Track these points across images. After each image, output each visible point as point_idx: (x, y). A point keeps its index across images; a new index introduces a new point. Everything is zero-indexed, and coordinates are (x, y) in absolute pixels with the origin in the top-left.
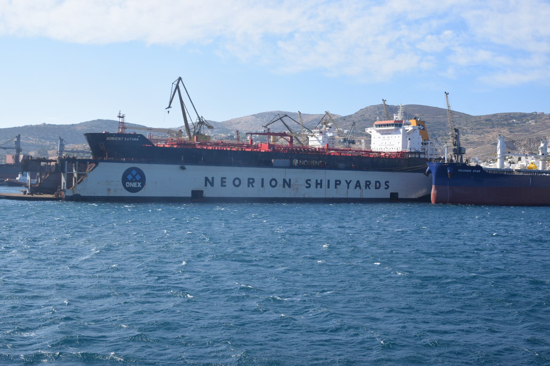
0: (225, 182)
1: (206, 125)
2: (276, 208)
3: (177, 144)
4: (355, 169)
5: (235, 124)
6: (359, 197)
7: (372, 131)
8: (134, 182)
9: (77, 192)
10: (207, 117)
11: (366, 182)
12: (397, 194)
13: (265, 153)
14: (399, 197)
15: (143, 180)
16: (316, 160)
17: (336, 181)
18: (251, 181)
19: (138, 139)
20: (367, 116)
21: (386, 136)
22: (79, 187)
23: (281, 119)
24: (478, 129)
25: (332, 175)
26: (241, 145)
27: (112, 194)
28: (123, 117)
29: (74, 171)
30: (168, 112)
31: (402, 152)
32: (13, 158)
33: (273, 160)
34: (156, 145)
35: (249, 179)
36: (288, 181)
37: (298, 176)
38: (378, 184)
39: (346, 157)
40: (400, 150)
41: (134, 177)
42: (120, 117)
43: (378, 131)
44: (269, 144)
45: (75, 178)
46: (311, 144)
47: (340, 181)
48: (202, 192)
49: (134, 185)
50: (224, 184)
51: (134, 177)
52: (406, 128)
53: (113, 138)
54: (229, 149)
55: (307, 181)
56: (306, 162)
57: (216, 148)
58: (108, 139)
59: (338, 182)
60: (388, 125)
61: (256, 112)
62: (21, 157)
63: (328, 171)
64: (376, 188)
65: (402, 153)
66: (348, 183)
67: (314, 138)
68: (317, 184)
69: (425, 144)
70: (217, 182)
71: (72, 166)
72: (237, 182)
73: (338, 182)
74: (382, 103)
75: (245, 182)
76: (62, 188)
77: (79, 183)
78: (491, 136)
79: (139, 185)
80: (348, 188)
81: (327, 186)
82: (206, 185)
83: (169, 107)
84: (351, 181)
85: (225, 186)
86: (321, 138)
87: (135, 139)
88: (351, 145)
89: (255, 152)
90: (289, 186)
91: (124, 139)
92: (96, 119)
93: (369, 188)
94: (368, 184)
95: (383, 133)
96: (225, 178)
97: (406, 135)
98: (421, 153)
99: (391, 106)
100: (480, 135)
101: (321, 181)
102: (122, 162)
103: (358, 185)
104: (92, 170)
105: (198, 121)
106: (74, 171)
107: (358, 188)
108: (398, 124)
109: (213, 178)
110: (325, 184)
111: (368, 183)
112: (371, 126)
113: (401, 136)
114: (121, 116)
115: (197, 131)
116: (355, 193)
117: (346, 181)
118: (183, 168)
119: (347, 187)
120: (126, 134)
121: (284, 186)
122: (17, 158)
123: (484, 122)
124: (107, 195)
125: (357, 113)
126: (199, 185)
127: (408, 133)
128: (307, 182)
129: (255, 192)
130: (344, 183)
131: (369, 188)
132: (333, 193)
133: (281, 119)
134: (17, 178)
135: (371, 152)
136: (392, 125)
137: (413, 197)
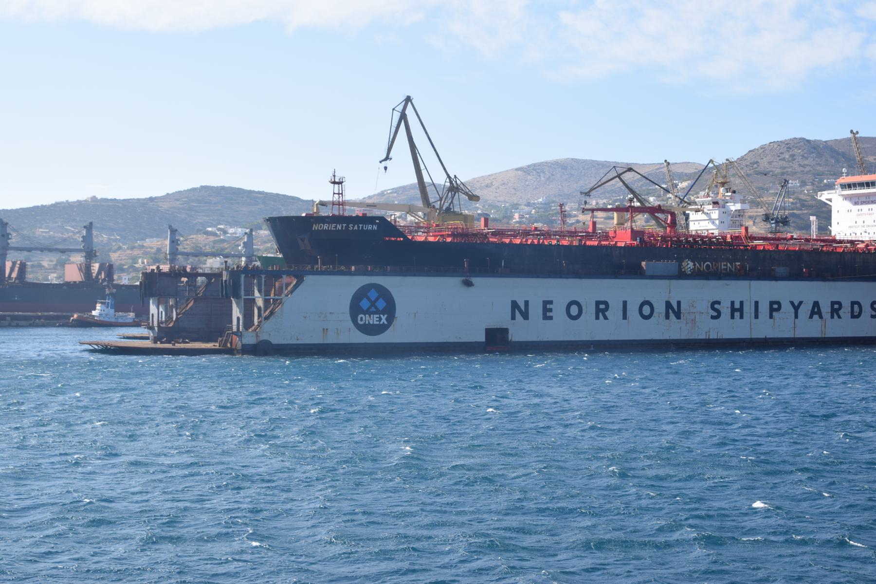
0: (551, 310)
1: (466, 194)
2: (833, 357)
3: (453, 235)
4: (810, 277)
5: (481, 188)
6: (819, 335)
8: (374, 313)
9: (264, 337)
10: (464, 177)
11: (833, 303)
13: (627, 248)
15: (390, 310)
16: (728, 260)
17: (772, 303)
18: (602, 306)
19: (375, 227)
20: (764, 165)
21: (865, 208)
22: (268, 325)
23: (619, 176)
25: (763, 291)
26: (573, 234)
27: (332, 339)
28: (340, 183)
29: (257, 294)
30: (386, 168)
32: (80, 269)
33: (643, 264)
34: (410, 237)
35: (598, 303)
36: (675, 307)
37: (697, 295)
38: (856, 307)
39: (788, 253)
41: (373, 303)
42: (334, 183)
44: (632, 229)
45: (259, 309)
46: (693, 227)
47: (778, 303)
48: (504, 331)
49: (374, 320)
50: (549, 314)
51: (373, 303)
53: (326, 227)
54: (554, 242)
55: (714, 304)
57: (529, 242)
58: (315, 227)
59: (775, 306)
61: (524, 163)
62: (96, 267)
63: (755, 284)
66: (796, 308)
67: (700, 216)
68: (733, 310)
70: (536, 310)
71: (252, 284)
72: (574, 310)
73: (775, 306)
74: (850, 135)
75: (590, 310)
76: (235, 329)
77: (267, 318)
79: (384, 320)
80: (796, 317)
81: (753, 315)
82: (513, 317)
83: (387, 158)
84: (801, 303)
85: (551, 318)
86: (715, 215)
87: (370, 227)
88: (781, 227)
89: (605, 246)
90: (678, 315)
91: (347, 227)
92: (198, 186)
93: (839, 317)
94: (836, 309)
95: (857, 201)
96: (551, 302)
99: (815, 141)
101: (742, 303)
102: (350, 273)
103: (816, 310)
104: (292, 292)
105: (448, 184)
106: (257, 294)
107: (816, 317)
109: (527, 303)
110: (748, 309)
111: (836, 306)
112: (830, 187)
114: (337, 180)
115: (446, 205)
116: (809, 328)
117: (792, 303)
118: (468, 284)
120: (350, 217)
121: (667, 317)
122: (86, 270)
124: (321, 342)
125: (742, 159)
126: (500, 317)
129: (610, 329)
131: (839, 317)
132: (764, 329)
133: (619, 176)
134: (94, 313)
135: (834, 241)
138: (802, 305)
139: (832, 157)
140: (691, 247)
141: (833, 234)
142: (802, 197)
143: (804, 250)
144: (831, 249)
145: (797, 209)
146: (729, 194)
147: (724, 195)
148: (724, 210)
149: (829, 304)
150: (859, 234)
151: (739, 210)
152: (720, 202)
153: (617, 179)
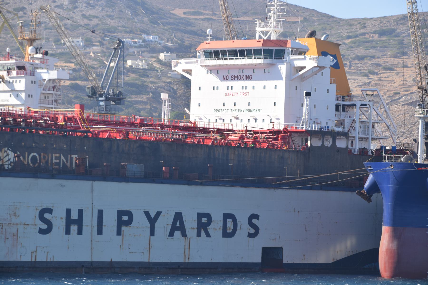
6: (181, 260)
7: (197, 70)
11: (200, 216)
12: (279, 250)
14: (286, 260)
16: (61, 151)
17: (120, 213)
21: (237, 85)
24: (361, 58)
31: (285, 131)
38: (230, 222)
39: (141, 143)
40: (280, 125)
43: (211, 70)
47: (129, 214)
52: (298, 64)
55: (44, 213)
56: (34, 158)
59: (125, 218)
60: (242, 53)
63: (99, 185)
64: (226, 235)
65: (287, 134)
66: (152, 220)
68: (69, 222)
69: (344, 108)
73: (125, 218)
78: (398, 80)
80: (152, 233)
84: (158, 214)
86: (20, 84)
93: (208, 235)
95: (226, 75)
97: (296, 77)
98: (338, 133)
100: (366, 75)
101: (81, 212)
103: (178, 225)
107: (178, 234)
108: (274, 52)
110: (90, 221)
113: (281, 84)
117: (147, 213)
119: (148, 231)
123: (376, 37)
127: (303, 78)
128: (42, 218)
130: (140, 220)
131: (208, 235)
136: (257, 52)
137: (322, 258)
138: (161, 217)
139: (129, 7)
140: (12, 130)
141: (192, 119)
142: (87, 61)
143: (161, 141)
144: (196, 141)
145: (81, 79)
146: (40, 56)
147: (33, 58)
148: (32, 78)
149: (196, 218)
150: (245, 122)
151: (53, 80)
152: (29, 68)
153: (209, 54)
